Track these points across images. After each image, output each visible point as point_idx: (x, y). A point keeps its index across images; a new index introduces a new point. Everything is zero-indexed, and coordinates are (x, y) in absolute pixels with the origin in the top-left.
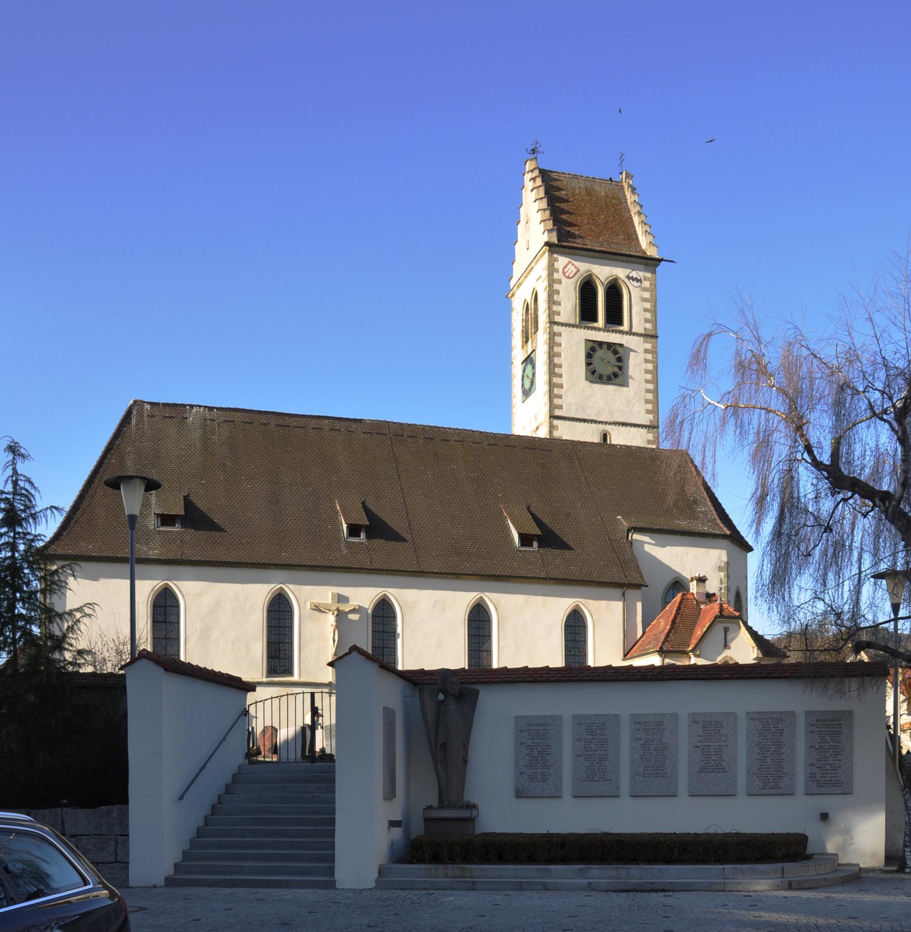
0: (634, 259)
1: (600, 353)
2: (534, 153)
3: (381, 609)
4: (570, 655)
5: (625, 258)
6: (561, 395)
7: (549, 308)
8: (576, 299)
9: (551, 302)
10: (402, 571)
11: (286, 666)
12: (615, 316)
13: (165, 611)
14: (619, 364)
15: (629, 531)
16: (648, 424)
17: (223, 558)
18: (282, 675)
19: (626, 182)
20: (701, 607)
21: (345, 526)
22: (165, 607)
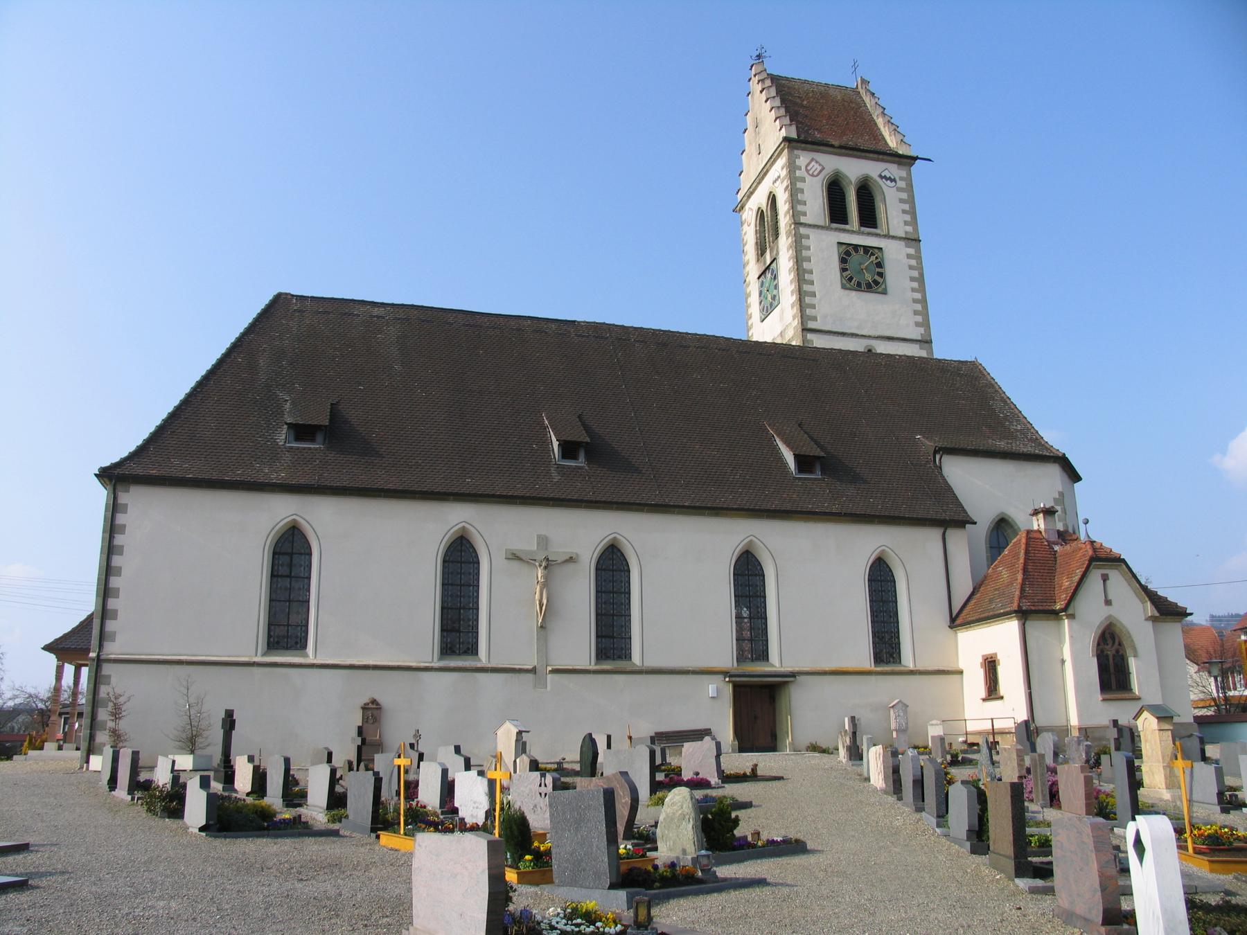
0: (885, 157)
1: (855, 258)
2: (759, 59)
3: (610, 559)
4: (877, 622)
5: (876, 156)
6: (815, 305)
7: (792, 208)
8: (823, 199)
9: (794, 201)
10: (639, 504)
11: (469, 643)
12: (869, 218)
13: (291, 561)
14: (879, 270)
15: (935, 452)
16: (920, 338)
17: (380, 484)
18: (463, 657)
19: (862, 88)
20: (1055, 549)
21: (556, 444)
22: (291, 555)
